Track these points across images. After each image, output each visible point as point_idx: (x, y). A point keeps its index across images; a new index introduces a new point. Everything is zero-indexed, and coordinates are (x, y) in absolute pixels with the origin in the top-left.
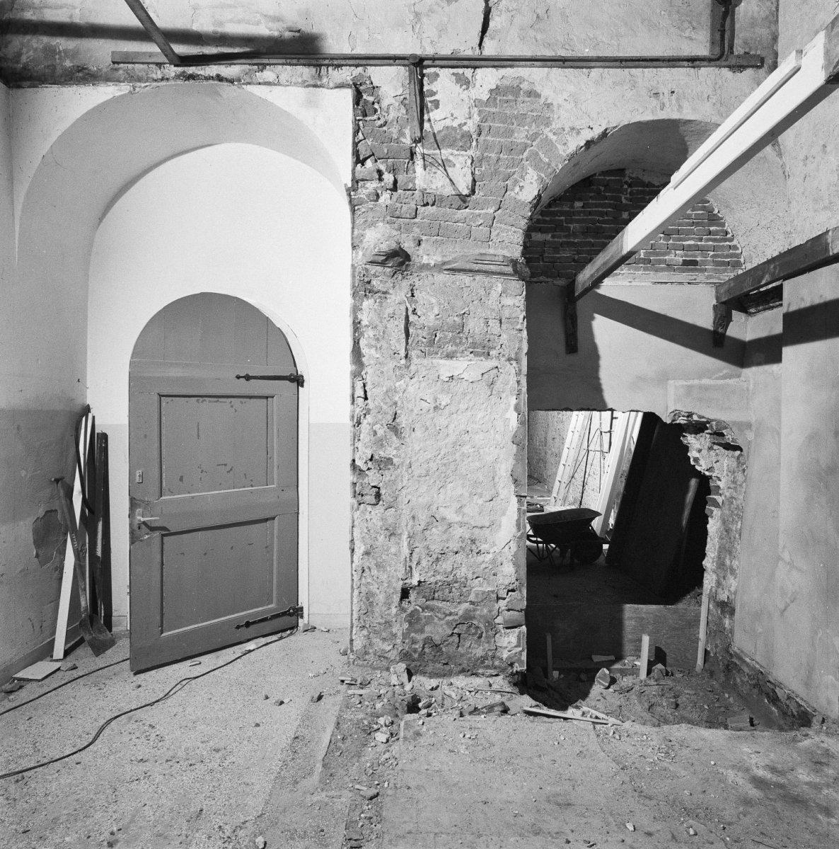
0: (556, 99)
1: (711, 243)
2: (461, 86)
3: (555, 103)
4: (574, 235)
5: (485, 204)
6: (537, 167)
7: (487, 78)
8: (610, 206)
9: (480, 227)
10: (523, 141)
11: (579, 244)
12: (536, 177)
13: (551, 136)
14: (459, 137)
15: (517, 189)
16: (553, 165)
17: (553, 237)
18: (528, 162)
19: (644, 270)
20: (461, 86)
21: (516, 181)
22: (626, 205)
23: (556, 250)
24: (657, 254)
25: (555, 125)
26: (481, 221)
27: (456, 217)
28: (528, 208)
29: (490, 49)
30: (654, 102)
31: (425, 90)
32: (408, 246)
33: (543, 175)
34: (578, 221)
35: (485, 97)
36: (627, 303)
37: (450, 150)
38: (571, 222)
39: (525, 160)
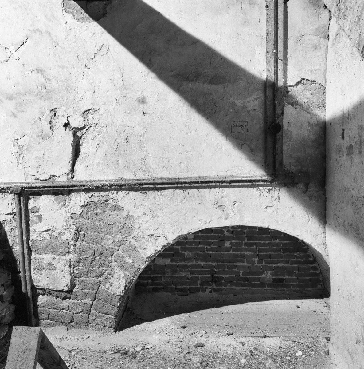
0: (137, 213)
1: (296, 265)
2: (58, 204)
3: (135, 216)
4: (188, 260)
5: (84, 296)
6: (123, 267)
7: (78, 200)
8: (215, 238)
9: (80, 314)
10: (111, 246)
11: (192, 266)
12: (122, 276)
13: (133, 242)
14: (59, 244)
15: (108, 285)
16: (136, 265)
17: (172, 261)
18: (116, 263)
19: (243, 286)
20: (58, 204)
21: (107, 279)
22: (228, 236)
23: (174, 271)
24: (253, 274)
25: (135, 233)
26: (81, 310)
27: (61, 305)
28: (117, 300)
29: (82, 175)
30: (219, 212)
31: (29, 207)
32: (57, 269)
33: (128, 274)
34: (190, 249)
35: (78, 211)
36: (277, 231)
37: (52, 256)
38: (185, 249)
39: (113, 261)
